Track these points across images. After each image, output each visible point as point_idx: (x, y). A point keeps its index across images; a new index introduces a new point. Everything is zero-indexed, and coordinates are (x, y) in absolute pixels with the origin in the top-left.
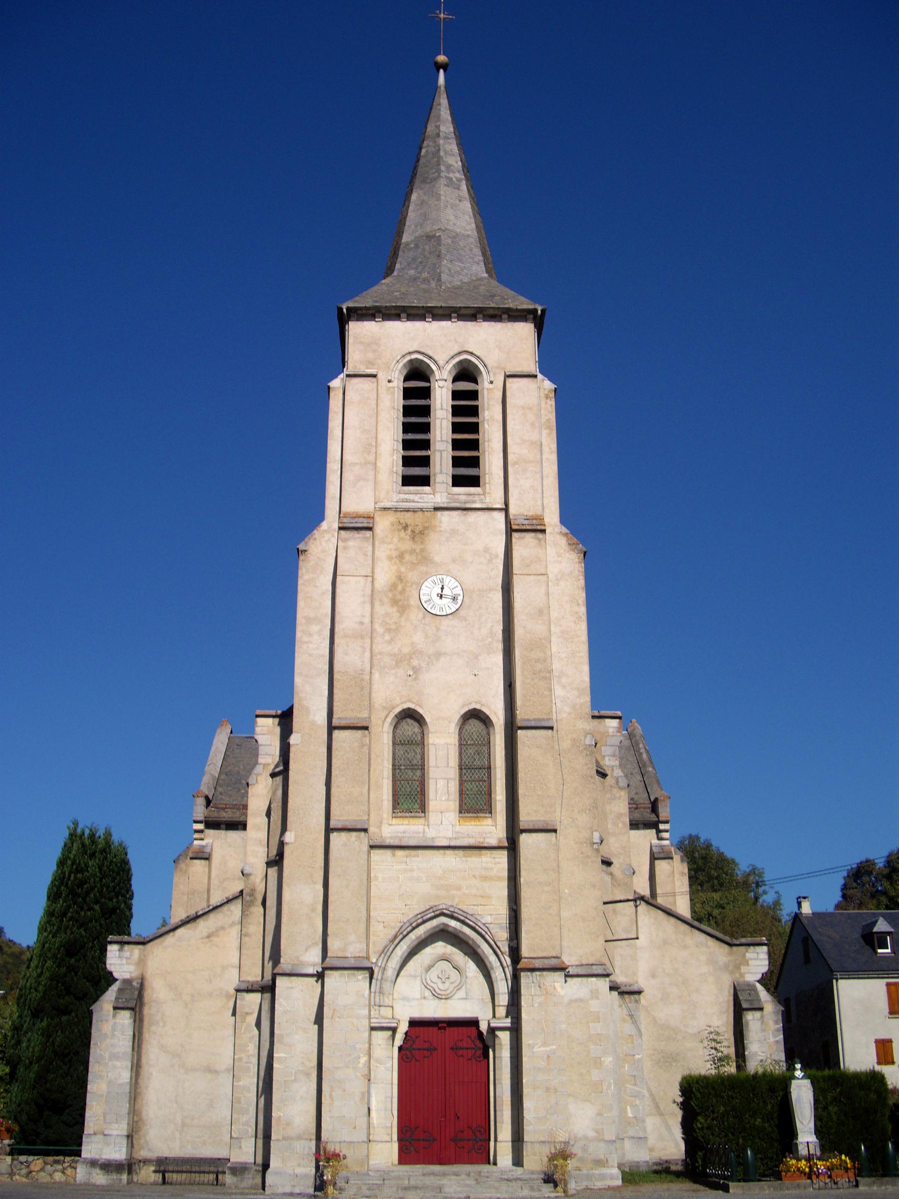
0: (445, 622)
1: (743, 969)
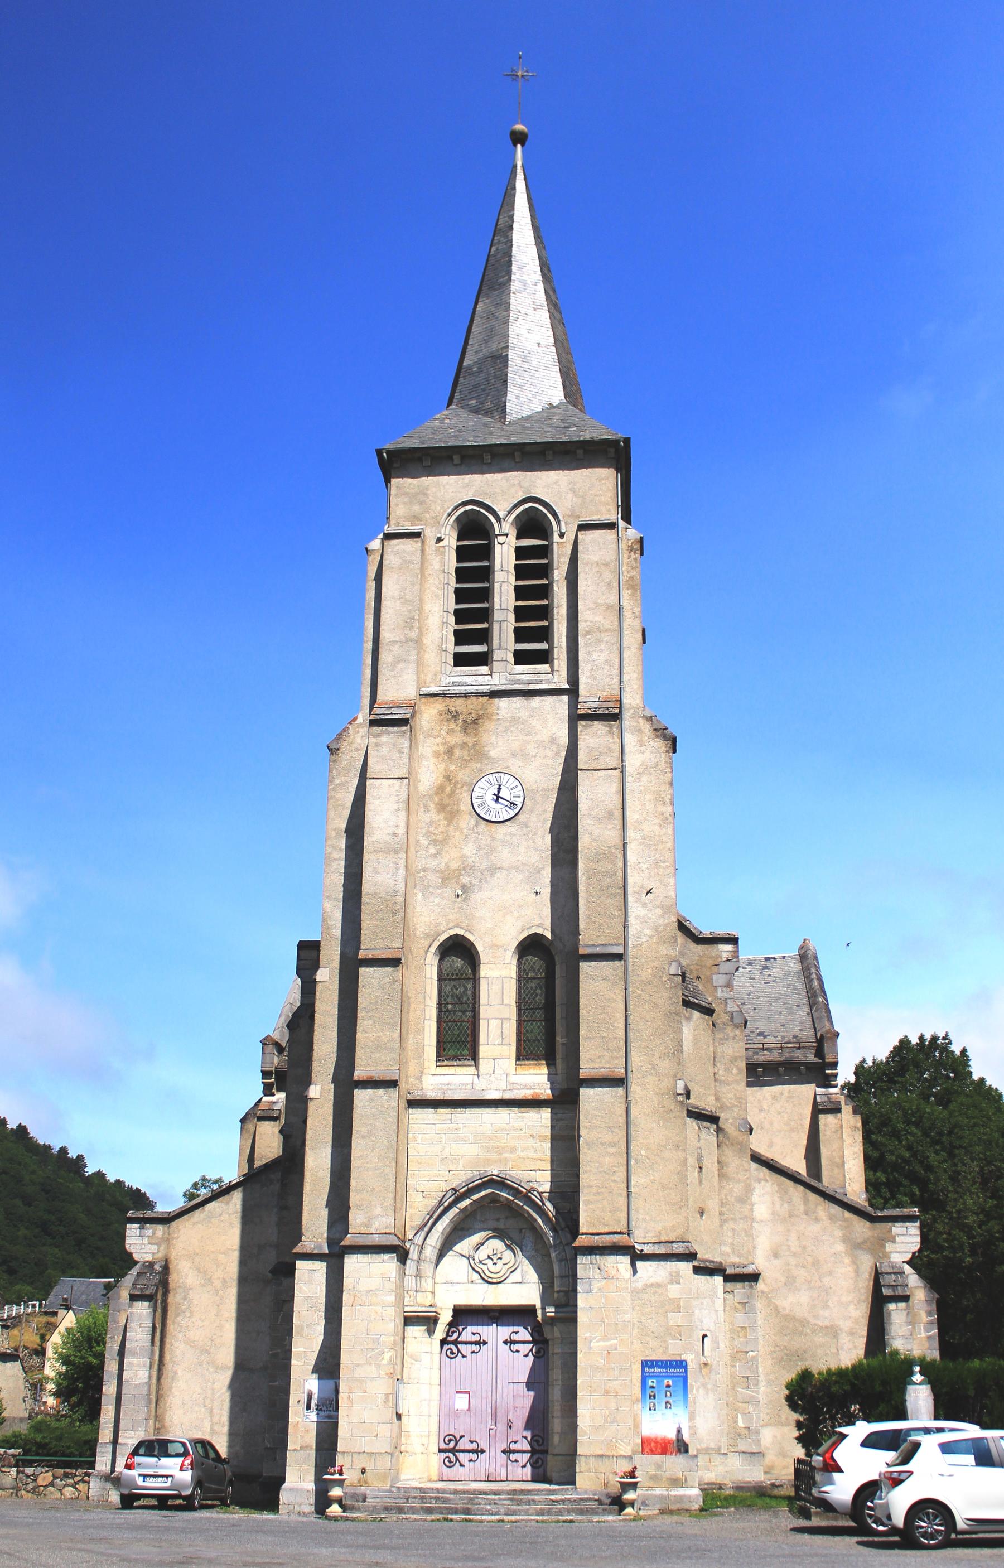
0: (502, 829)
1: (889, 1247)
